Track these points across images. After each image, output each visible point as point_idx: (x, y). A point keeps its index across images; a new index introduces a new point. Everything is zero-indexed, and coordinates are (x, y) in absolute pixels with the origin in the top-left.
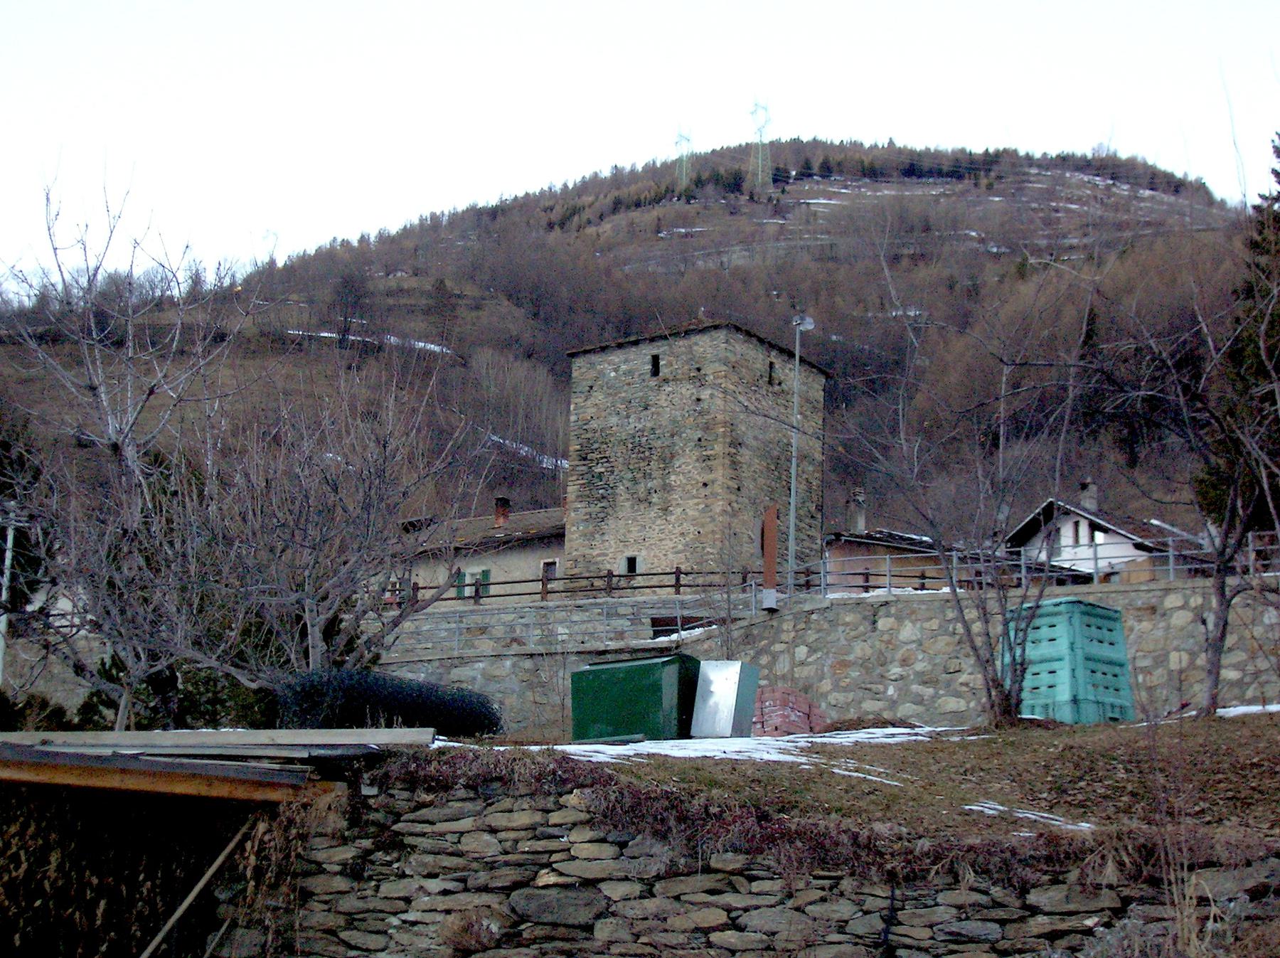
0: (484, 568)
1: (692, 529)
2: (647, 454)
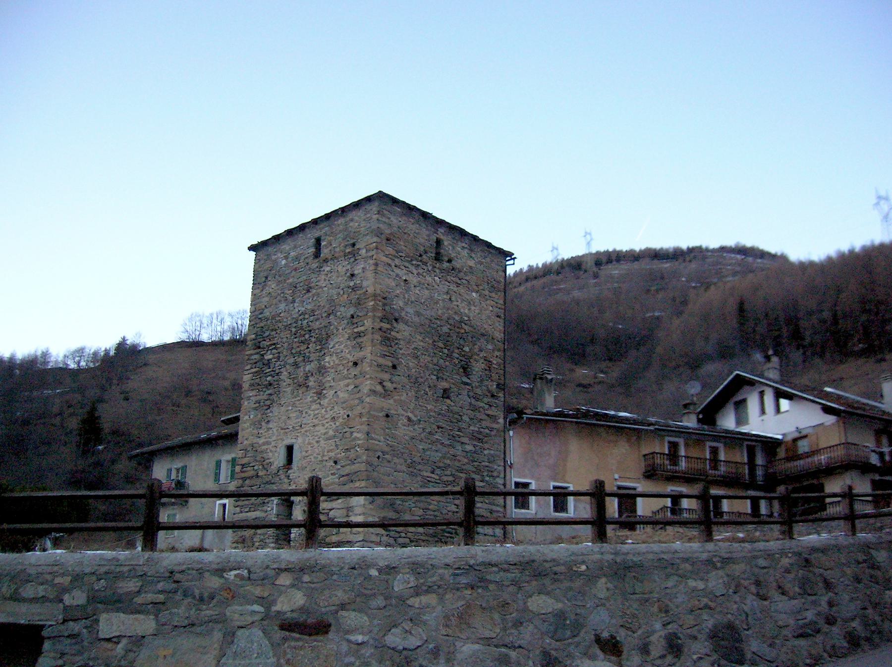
0: (233, 455)
1: (342, 412)
2: (307, 336)
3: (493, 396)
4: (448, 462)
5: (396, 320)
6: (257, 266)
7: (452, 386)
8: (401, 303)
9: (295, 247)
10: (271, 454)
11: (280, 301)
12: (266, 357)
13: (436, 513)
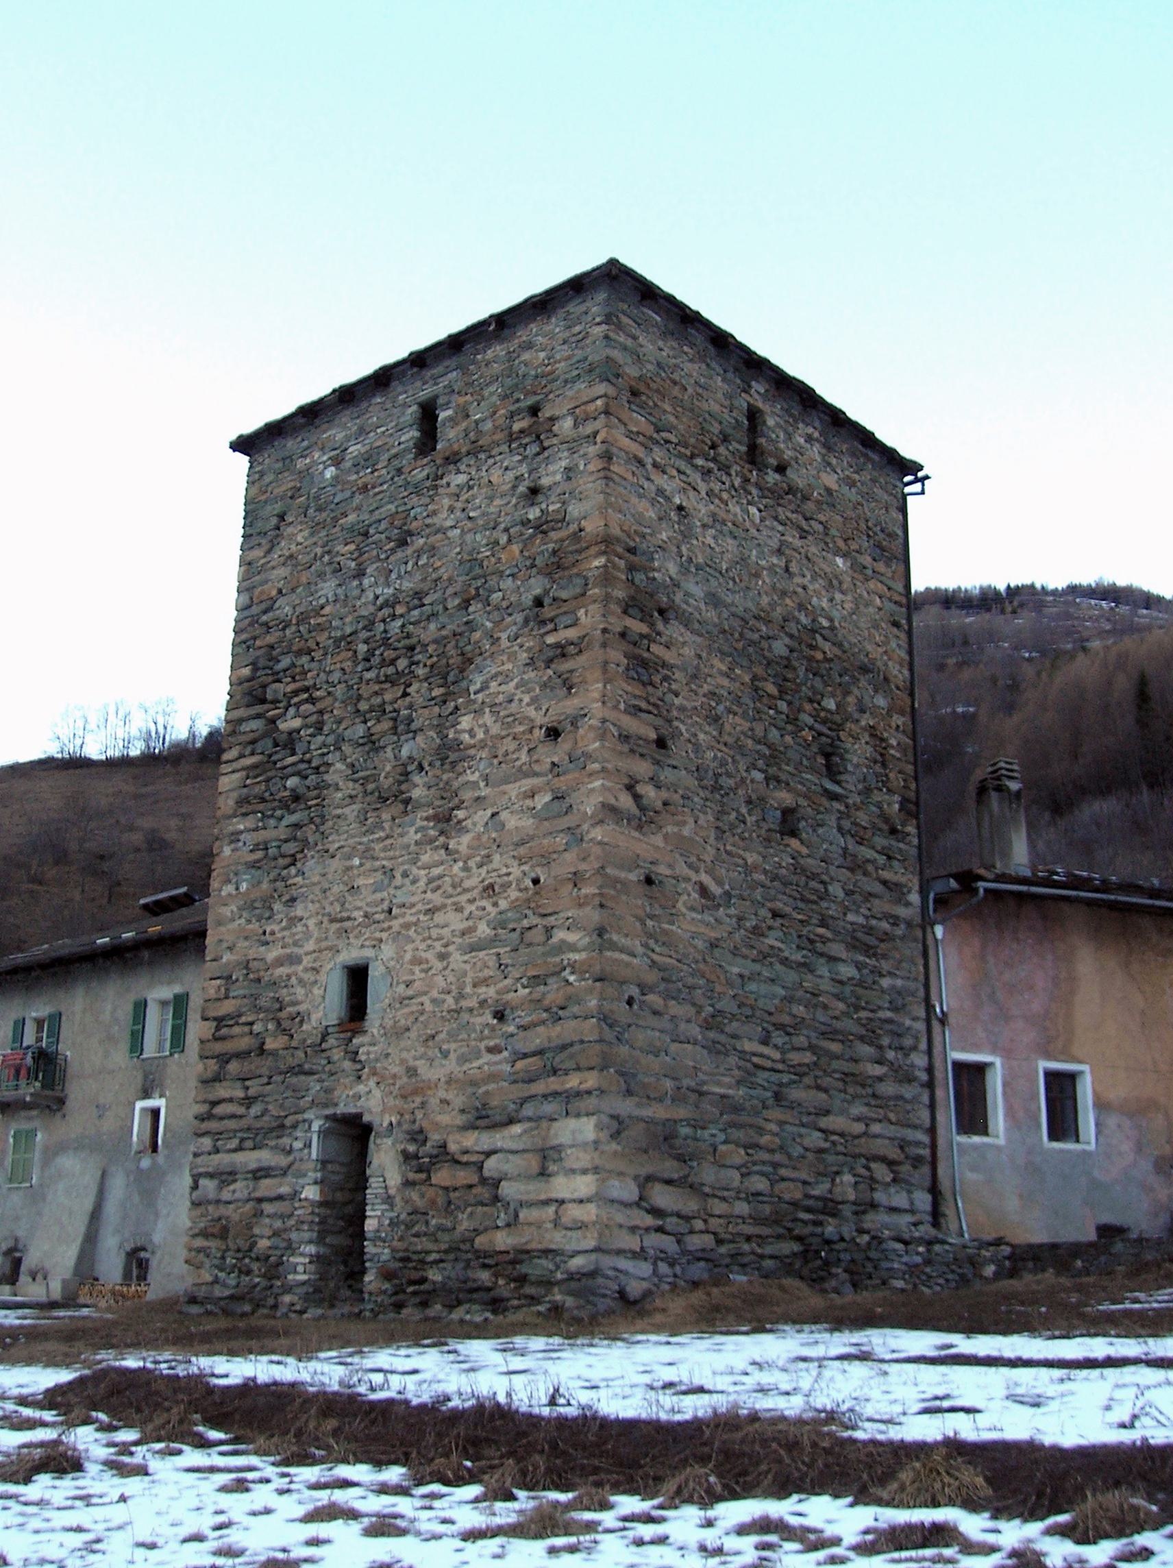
0: (178, 989)
1: (516, 871)
2: (402, 664)
3: (893, 831)
4: (800, 1010)
5: (661, 612)
6: (254, 490)
7: (803, 802)
8: (673, 569)
9: (362, 431)
10: (300, 991)
11: (321, 575)
12: (283, 726)
13: (778, 1157)
